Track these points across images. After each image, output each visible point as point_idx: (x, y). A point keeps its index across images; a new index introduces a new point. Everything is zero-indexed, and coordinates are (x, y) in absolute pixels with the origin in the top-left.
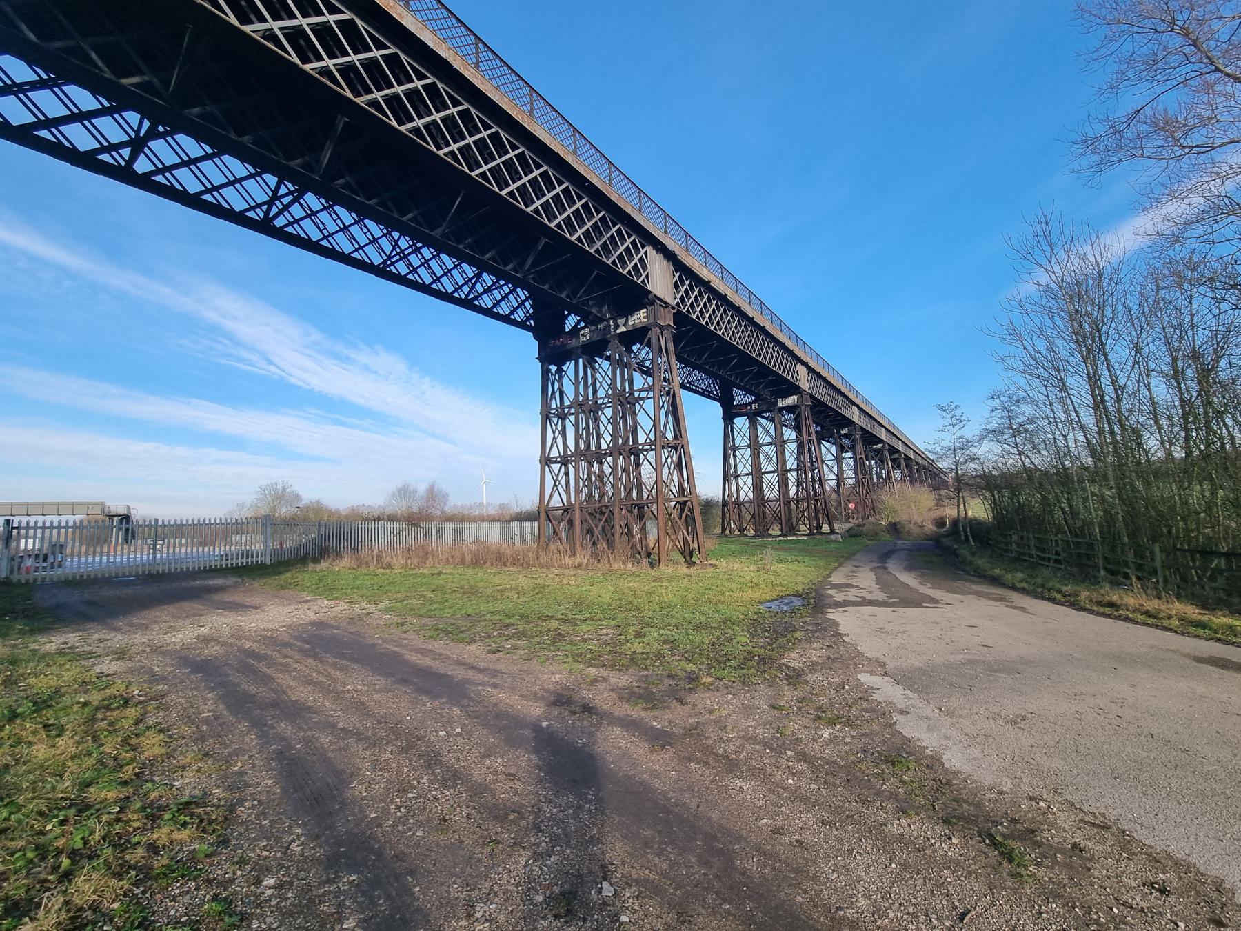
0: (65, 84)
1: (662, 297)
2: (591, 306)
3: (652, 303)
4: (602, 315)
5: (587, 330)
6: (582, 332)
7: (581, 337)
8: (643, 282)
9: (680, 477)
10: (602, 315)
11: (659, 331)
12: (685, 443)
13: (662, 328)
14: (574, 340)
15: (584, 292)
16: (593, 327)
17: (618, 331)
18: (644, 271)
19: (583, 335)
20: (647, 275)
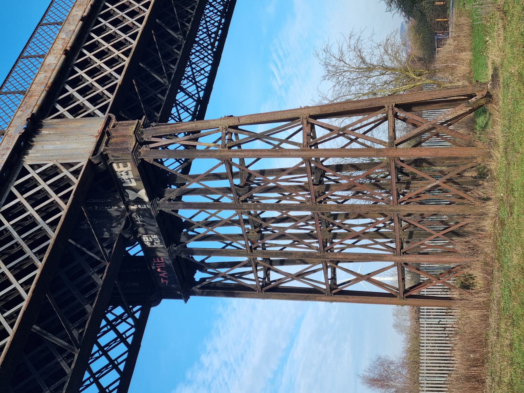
0: (113, 309)
1: (95, 140)
2: (111, 234)
3: (105, 157)
4: (123, 216)
5: (145, 238)
6: (148, 244)
7: (155, 245)
8: (75, 173)
9: (240, 265)
10: (123, 216)
11: (144, 148)
12: (306, 113)
13: (141, 143)
14: (159, 254)
15: (90, 250)
16: (141, 230)
17: (146, 199)
18: (70, 111)
19: (152, 243)
20: (64, 165)
